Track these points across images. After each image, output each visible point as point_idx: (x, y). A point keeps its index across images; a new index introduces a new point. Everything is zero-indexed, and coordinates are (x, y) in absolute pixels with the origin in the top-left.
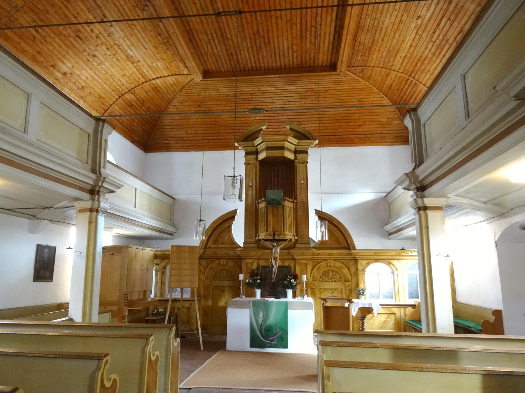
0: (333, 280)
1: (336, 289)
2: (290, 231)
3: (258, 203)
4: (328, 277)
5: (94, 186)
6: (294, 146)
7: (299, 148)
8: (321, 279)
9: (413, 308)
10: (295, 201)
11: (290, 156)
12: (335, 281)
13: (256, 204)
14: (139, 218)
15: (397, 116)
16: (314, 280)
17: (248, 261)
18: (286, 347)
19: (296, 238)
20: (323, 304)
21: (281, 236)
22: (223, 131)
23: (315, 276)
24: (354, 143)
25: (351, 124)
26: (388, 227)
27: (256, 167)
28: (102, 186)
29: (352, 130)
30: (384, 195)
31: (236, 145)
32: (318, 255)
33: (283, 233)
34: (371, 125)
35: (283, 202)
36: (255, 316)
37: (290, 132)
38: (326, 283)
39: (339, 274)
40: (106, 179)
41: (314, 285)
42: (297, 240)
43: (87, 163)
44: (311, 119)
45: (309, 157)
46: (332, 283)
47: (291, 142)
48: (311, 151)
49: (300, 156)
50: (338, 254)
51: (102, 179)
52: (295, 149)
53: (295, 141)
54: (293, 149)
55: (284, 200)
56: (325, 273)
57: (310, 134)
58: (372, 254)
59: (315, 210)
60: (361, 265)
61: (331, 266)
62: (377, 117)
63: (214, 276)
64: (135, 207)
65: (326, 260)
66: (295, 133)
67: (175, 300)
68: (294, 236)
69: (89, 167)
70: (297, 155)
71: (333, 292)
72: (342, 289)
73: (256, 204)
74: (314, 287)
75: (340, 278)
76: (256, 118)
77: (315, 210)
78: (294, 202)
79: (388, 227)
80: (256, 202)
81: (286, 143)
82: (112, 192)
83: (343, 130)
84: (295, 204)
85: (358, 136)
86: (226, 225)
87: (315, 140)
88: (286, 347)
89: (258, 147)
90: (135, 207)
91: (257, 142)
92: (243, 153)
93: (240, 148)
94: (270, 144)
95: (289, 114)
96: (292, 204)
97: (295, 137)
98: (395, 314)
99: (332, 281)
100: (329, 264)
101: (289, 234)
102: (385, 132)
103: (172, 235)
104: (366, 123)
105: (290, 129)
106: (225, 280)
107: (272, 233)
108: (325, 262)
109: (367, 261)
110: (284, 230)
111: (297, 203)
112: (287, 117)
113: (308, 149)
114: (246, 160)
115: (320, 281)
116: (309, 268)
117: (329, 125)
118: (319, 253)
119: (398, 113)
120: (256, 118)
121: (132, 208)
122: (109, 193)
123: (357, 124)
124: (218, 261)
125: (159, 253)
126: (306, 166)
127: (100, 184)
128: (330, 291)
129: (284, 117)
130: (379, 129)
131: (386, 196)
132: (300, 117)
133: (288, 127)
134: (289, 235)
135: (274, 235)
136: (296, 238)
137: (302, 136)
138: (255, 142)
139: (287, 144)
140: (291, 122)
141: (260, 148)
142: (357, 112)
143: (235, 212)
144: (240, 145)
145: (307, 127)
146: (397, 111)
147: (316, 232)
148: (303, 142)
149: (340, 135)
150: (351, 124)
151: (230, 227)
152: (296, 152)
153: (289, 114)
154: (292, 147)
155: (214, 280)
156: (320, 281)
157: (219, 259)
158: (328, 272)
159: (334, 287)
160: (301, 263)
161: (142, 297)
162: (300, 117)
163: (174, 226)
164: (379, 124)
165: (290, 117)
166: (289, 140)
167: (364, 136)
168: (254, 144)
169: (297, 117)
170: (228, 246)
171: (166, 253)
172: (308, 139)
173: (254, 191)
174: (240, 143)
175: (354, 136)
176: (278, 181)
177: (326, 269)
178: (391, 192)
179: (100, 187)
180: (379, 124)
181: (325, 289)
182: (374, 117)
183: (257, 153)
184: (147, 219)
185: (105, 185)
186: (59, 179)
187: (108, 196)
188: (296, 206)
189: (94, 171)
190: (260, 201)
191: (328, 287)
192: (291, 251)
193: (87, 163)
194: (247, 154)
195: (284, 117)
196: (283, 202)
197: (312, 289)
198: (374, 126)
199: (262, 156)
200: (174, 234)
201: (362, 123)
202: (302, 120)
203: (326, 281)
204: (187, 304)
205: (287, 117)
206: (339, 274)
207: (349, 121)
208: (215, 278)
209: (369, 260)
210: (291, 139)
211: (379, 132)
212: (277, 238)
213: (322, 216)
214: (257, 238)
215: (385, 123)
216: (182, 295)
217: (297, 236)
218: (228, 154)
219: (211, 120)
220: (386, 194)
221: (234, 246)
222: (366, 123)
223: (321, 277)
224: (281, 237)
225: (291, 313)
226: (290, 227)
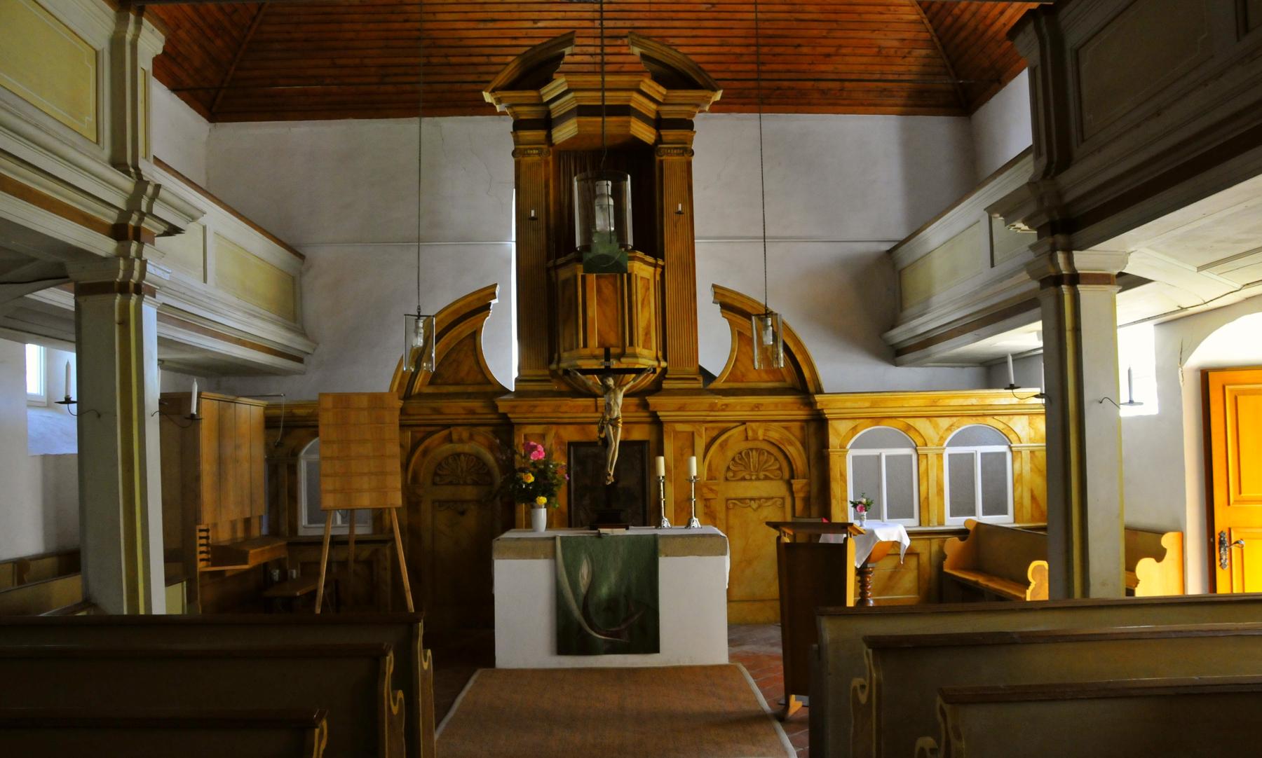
0: (761, 475)
1: (768, 499)
2: (647, 345)
3: (557, 267)
4: (747, 467)
5: (125, 215)
6: (653, 106)
7: (669, 112)
8: (731, 474)
9: (962, 539)
10: (660, 262)
11: (645, 133)
12: (766, 478)
13: (548, 270)
14: (220, 314)
15: (923, 35)
16: (711, 478)
17: (529, 429)
18: (655, 648)
19: (663, 364)
20: (779, 538)
21: (623, 360)
22: (443, 60)
23: (714, 467)
24: (809, 104)
25: (805, 50)
26: (899, 334)
27: (547, 163)
28: (150, 213)
29: (804, 67)
30: (886, 247)
31: (488, 97)
32: (723, 410)
33: (628, 350)
34: (855, 55)
35: (629, 264)
36: (569, 574)
37: (642, 67)
38: (743, 483)
39: (776, 459)
40: (162, 193)
41: (711, 490)
42: (665, 370)
43: (97, 142)
44: (695, 33)
45: (695, 138)
46: (758, 483)
47: (649, 95)
48: (698, 120)
49: (669, 135)
50: (776, 405)
51: (150, 190)
52: (658, 113)
53: (658, 91)
54: (652, 116)
55: (632, 259)
56: (741, 459)
57: (700, 71)
58: (867, 404)
59: (714, 286)
60: (837, 434)
61: (755, 439)
62: (875, 35)
63: (436, 474)
64: (205, 281)
65: (744, 423)
66: (655, 67)
67: (337, 542)
68: (657, 359)
69: (107, 153)
70: (663, 132)
71: (760, 506)
72: (783, 498)
73: (548, 270)
74: (710, 496)
75: (780, 469)
76: (540, 24)
77: (714, 286)
78: (655, 266)
79: (899, 334)
80: (551, 263)
81: (635, 95)
82: (173, 230)
83: (781, 67)
84: (659, 270)
85: (823, 85)
86: (464, 329)
87: (714, 90)
88: (655, 648)
89: (552, 106)
90: (205, 281)
91: (549, 92)
92: (508, 123)
93: (498, 108)
94: (591, 98)
95: (634, 15)
96: (651, 269)
97: (657, 78)
98: (918, 555)
99: (758, 479)
100: (750, 433)
101: (645, 352)
102: (890, 77)
103: (300, 360)
104: (844, 51)
105: (643, 55)
106: (465, 484)
107: (601, 352)
108: (742, 428)
109: (851, 424)
110: (631, 344)
111: (663, 267)
112: (628, 24)
113: (693, 115)
114: (517, 142)
115: (727, 479)
116: (700, 444)
117: (744, 50)
118: (727, 405)
119: (929, 26)
120: (540, 24)
121: (197, 283)
122: (167, 234)
123: (819, 50)
124: (446, 432)
125: (282, 412)
126: (689, 164)
127: (144, 209)
128: (754, 505)
129: (620, 24)
130: (878, 68)
131: (890, 252)
132: (665, 24)
133: (637, 50)
134: (646, 357)
135: (608, 356)
136: (663, 364)
137: (674, 78)
138: (544, 90)
139: (637, 101)
140: (636, 35)
141: (557, 109)
142: (822, 17)
143: (490, 292)
144: (499, 101)
145: (686, 51)
146: (926, 21)
147: (714, 346)
148: (679, 94)
149: (776, 81)
150: (805, 50)
151: (475, 335)
152: (659, 123)
153: (634, 15)
154: (649, 108)
155: (434, 484)
156: (727, 479)
157: (447, 426)
158: (748, 454)
159: (765, 495)
160: (676, 433)
161: (240, 534)
162: (665, 24)
163: (302, 332)
164: (879, 54)
165: (637, 24)
166: (644, 88)
167: (836, 85)
168: (541, 97)
169: (658, 24)
170: (470, 389)
171: (299, 412)
172: (693, 85)
173: (543, 233)
174: (500, 94)
175: (809, 84)
176: (606, 206)
177: (744, 446)
178: (902, 243)
179: (142, 216)
180: (879, 54)
181: (742, 500)
182: (867, 34)
183: (547, 123)
184: (239, 315)
185: (158, 210)
186: (29, 190)
187: (162, 242)
188: (662, 275)
189: (118, 163)
190: (561, 261)
191: (749, 495)
192: (651, 400)
193: (97, 142)
194: (519, 125)
195: (620, 24)
196: (629, 264)
197: (707, 500)
198: (864, 60)
199: (565, 132)
200: (306, 359)
201: (832, 50)
202: (674, 32)
203: (744, 479)
204: (366, 553)
205: (628, 24)
206: (776, 459)
207: (799, 41)
208: (438, 479)
209: (858, 421)
210: (649, 85)
211: (877, 76)
212: (614, 364)
213: (730, 305)
214: (554, 366)
215: (892, 52)
216: (352, 528)
217: (665, 359)
218: (454, 128)
219: (408, 25)
220: (893, 244)
221: (489, 388)
222: (844, 51)
223: (728, 468)
224: (625, 363)
225: (668, 567)
226: (647, 333)
